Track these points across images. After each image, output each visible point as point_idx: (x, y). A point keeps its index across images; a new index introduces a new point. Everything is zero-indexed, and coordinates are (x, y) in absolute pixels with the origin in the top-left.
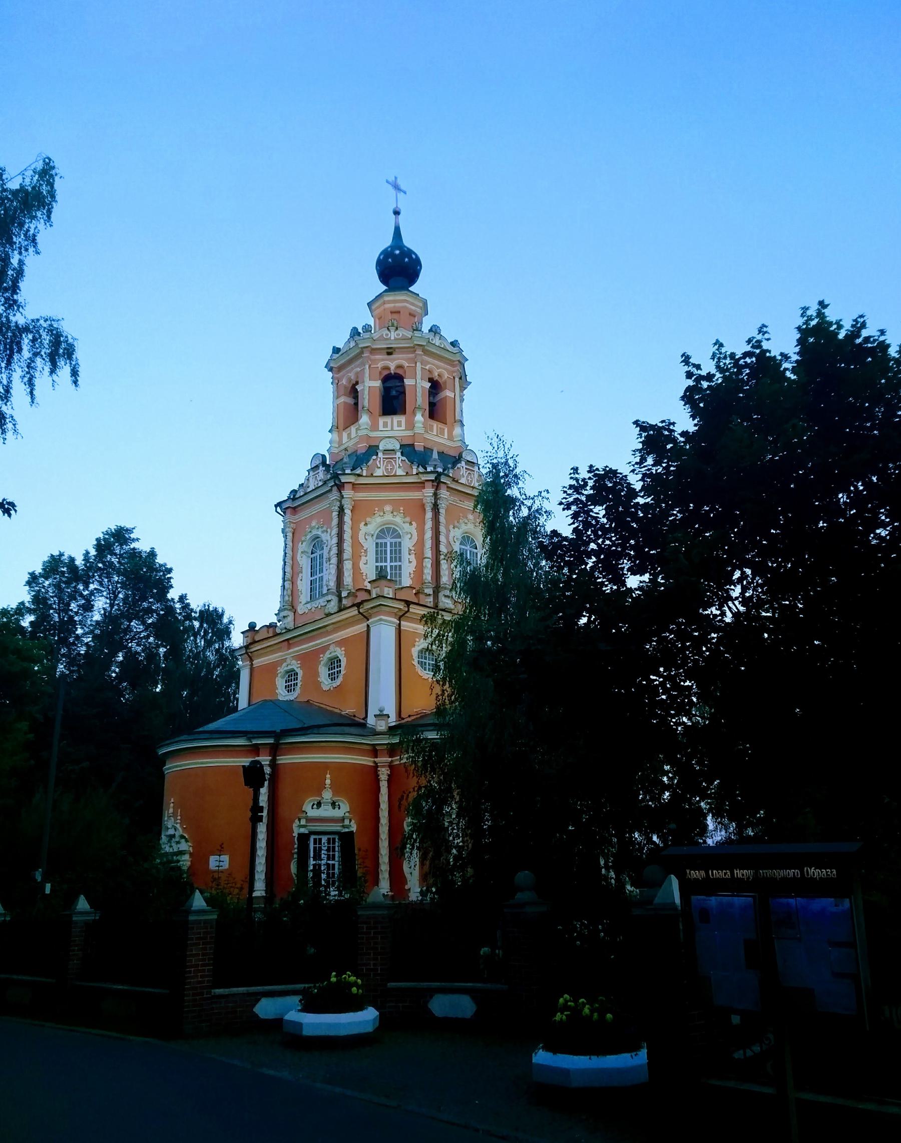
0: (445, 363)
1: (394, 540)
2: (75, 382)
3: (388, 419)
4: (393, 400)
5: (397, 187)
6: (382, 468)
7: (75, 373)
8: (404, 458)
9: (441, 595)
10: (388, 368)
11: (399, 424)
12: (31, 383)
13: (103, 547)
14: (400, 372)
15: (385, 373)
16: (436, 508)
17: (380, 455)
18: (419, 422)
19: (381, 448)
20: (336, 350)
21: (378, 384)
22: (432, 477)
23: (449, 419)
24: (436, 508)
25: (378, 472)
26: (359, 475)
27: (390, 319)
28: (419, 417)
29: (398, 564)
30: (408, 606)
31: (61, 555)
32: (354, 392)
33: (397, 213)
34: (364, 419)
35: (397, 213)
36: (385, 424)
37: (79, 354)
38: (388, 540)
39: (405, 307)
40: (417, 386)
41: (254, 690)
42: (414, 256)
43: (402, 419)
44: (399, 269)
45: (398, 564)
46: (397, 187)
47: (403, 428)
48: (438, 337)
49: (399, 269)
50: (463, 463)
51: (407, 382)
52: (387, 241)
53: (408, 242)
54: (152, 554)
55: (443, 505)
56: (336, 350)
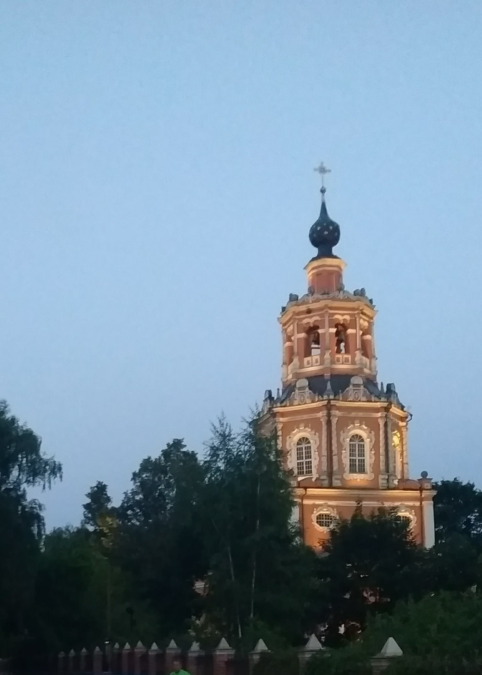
1: (307, 445)
2: (61, 480)
5: (322, 170)
7: (61, 477)
8: (311, 391)
9: (333, 478)
12: (50, 483)
13: (166, 454)
15: (308, 326)
16: (329, 423)
17: (297, 391)
19: (297, 386)
20: (293, 298)
22: (325, 402)
24: (329, 423)
26: (284, 406)
29: (299, 461)
30: (306, 490)
31: (149, 458)
33: (323, 191)
35: (323, 191)
37: (63, 470)
38: (304, 446)
39: (324, 270)
41: (312, 486)
44: (325, 236)
45: (299, 461)
46: (322, 170)
48: (341, 292)
49: (325, 236)
50: (351, 387)
52: (315, 216)
55: (334, 421)
56: (293, 298)
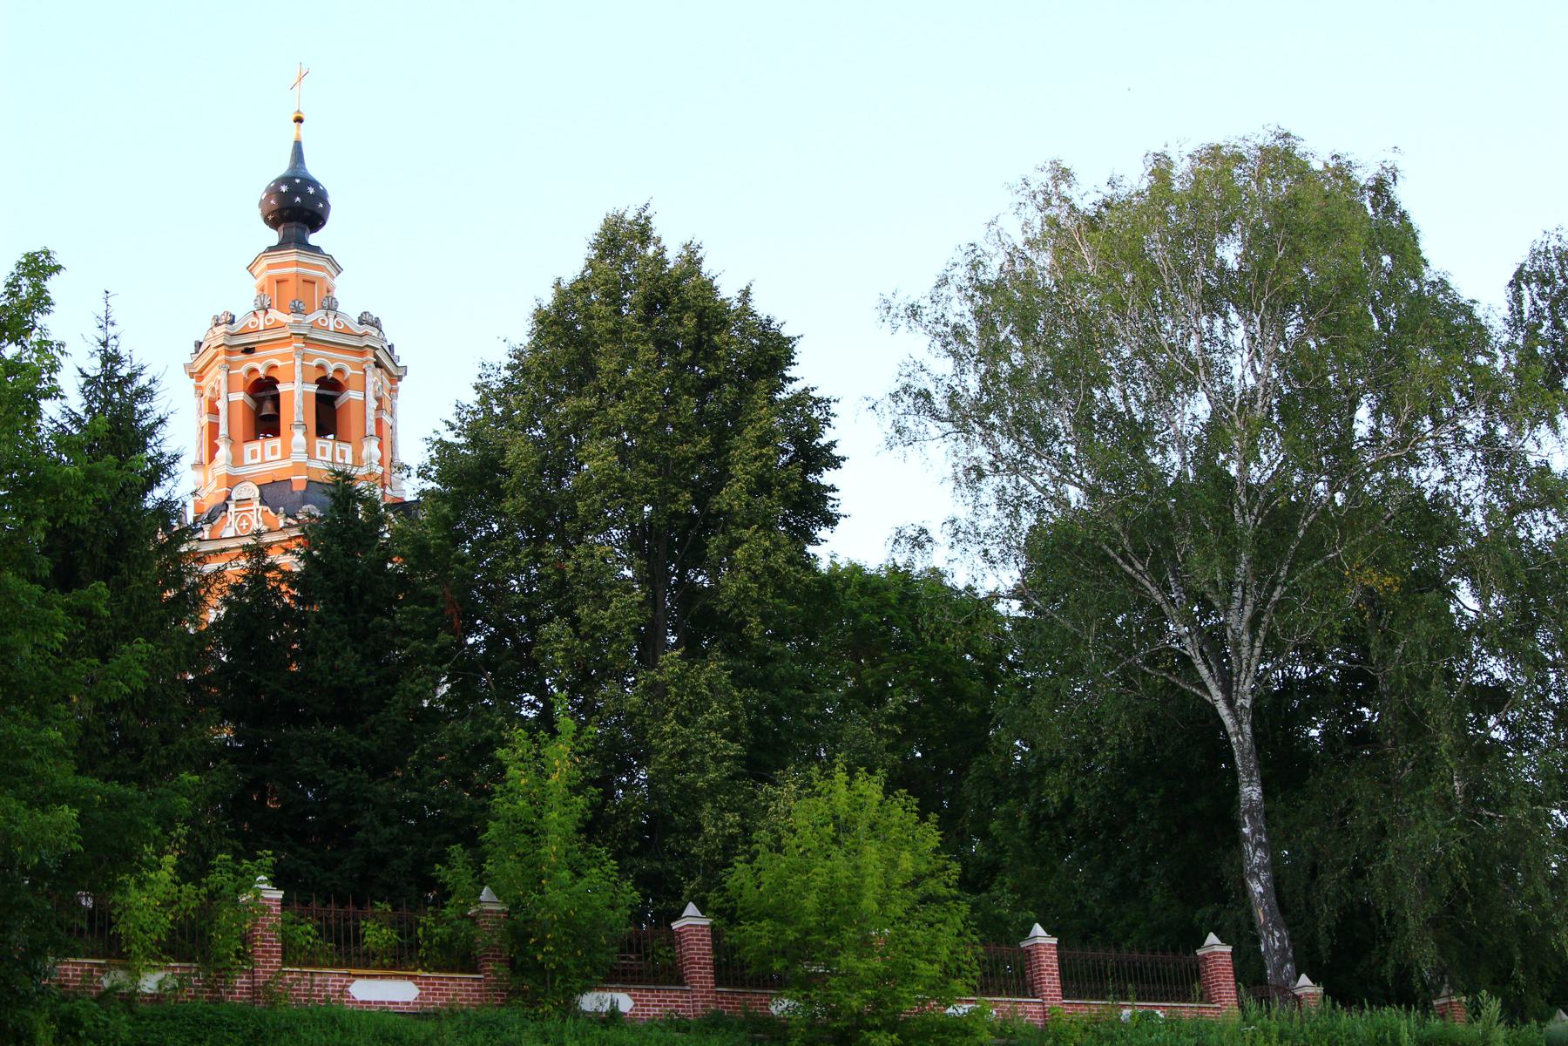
0: (344, 352)
3: (257, 445)
4: (264, 416)
6: (234, 524)
10: (254, 370)
11: (274, 451)
14: (339, 377)
18: (297, 446)
21: (239, 396)
23: (355, 432)
25: (230, 533)
27: (276, 292)
28: (299, 438)
32: (214, 411)
34: (224, 452)
36: (254, 455)
40: (297, 394)
42: (311, 191)
43: (277, 442)
44: (297, 209)
47: (279, 456)
49: (297, 209)
51: (281, 388)
52: (282, 167)
53: (313, 168)
54: (1161, 171)
